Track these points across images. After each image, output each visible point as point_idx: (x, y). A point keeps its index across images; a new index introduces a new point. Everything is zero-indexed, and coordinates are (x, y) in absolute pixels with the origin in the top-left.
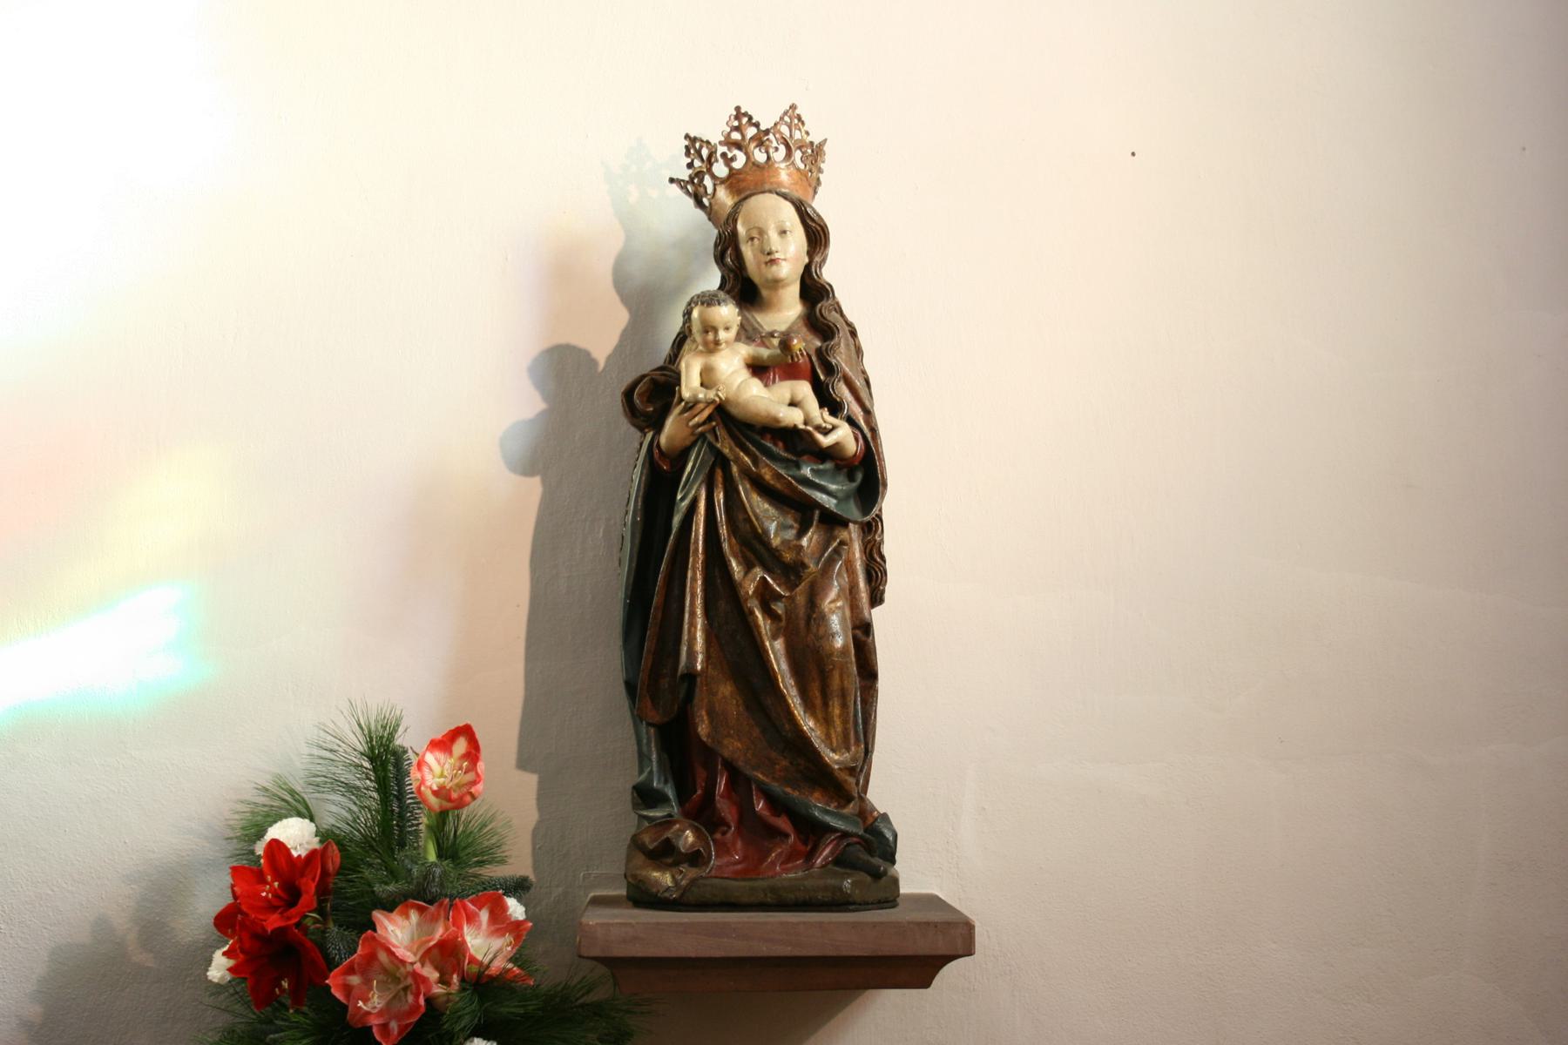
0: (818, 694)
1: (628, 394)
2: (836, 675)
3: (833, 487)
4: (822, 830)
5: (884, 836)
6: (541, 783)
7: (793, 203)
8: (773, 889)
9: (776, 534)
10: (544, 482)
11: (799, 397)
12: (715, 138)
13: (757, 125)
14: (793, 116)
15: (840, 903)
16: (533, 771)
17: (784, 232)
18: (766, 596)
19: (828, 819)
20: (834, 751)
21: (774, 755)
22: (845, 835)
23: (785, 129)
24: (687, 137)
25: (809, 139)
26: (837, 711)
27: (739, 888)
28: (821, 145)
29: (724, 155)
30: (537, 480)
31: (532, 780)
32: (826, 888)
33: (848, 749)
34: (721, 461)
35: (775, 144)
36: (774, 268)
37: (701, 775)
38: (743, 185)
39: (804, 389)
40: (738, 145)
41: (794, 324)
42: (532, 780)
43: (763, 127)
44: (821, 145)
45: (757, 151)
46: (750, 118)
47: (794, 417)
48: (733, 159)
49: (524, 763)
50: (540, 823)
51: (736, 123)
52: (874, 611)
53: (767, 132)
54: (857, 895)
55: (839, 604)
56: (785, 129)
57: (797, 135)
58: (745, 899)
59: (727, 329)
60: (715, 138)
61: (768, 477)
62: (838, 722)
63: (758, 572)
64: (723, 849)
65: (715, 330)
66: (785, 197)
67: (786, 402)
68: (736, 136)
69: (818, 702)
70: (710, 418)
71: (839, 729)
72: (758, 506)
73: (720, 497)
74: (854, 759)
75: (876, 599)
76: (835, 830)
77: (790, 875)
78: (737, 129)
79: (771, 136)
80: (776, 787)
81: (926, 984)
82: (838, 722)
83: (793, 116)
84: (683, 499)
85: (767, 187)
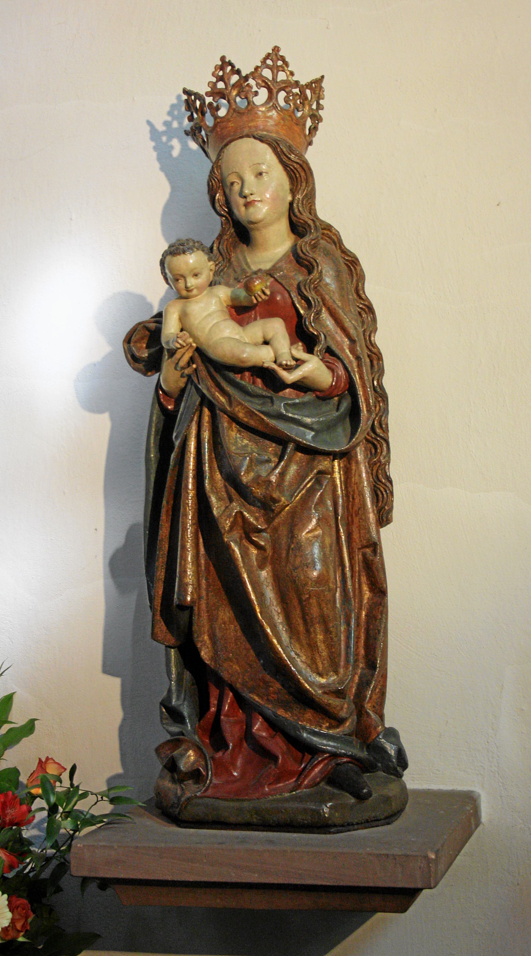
0: (300, 621)
1: (128, 340)
2: (313, 601)
3: (308, 420)
4: (313, 751)
5: (386, 752)
6: (123, 685)
7: (270, 145)
8: (257, 811)
9: (248, 471)
10: (112, 419)
11: (269, 336)
12: (203, 89)
13: (238, 72)
14: (275, 58)
15: (321, 826)
16: (117, 676)
17: (261, 174)
18: (248, 532)
19: (315, 739)
20: (321, 675)
21: (268, 678)
22: (334, 755)
23: (267, 73)
24: (185, 92)
25: (295, 78)
26: (320, 637)
27: (227, 808)
28: (316, 86)
29: (210, 104)
30: (106, 416)
31: (115, 683)
32: (305, 810)
33: (336, 672)
34: (206, 402)
35: (255, 89)
36: (251, 210)
37: (214, 692)
38: (225, 132)
39: (277, 328)
40: (222, 94)
41: (280, 260)
42: (115, 683)
43: (244, 74)
44: (316, 86)
45: (238, 99)
46: (233, 66)
47: (264, 356)
48: (218, 108)
49: (108, 669)
50: (124, 720)
51: (221, 73)
52: (382, 530)
53: (246, 78)
54: (337, 818)
55: (319, 532)
56: (267, 73)
57: (282, 76)
58: (232, 819)
59: (196, 275)
60: (203, 89)
61: (241, 415)
62: (322, 646)
63: (236, 507)
64: (222, 768)
65: (184, 277)
66: (261, 139)
67: (265, 343)
68: (221, 85)
69: (301, 628)
70: (192, 360)
71: (324, 654)
72: (236, 440)
73: (206, 435)
74: (341, 682)
75: (384, 518)
76: (324, 752)
77: (279, 795)
78: (221, 79)
79: (251, 82)
80: (269, 708)
81: (403, 909)
82: (322, 646)
83: (275, 58)
84: (177, 437)
85: (246, 131)
